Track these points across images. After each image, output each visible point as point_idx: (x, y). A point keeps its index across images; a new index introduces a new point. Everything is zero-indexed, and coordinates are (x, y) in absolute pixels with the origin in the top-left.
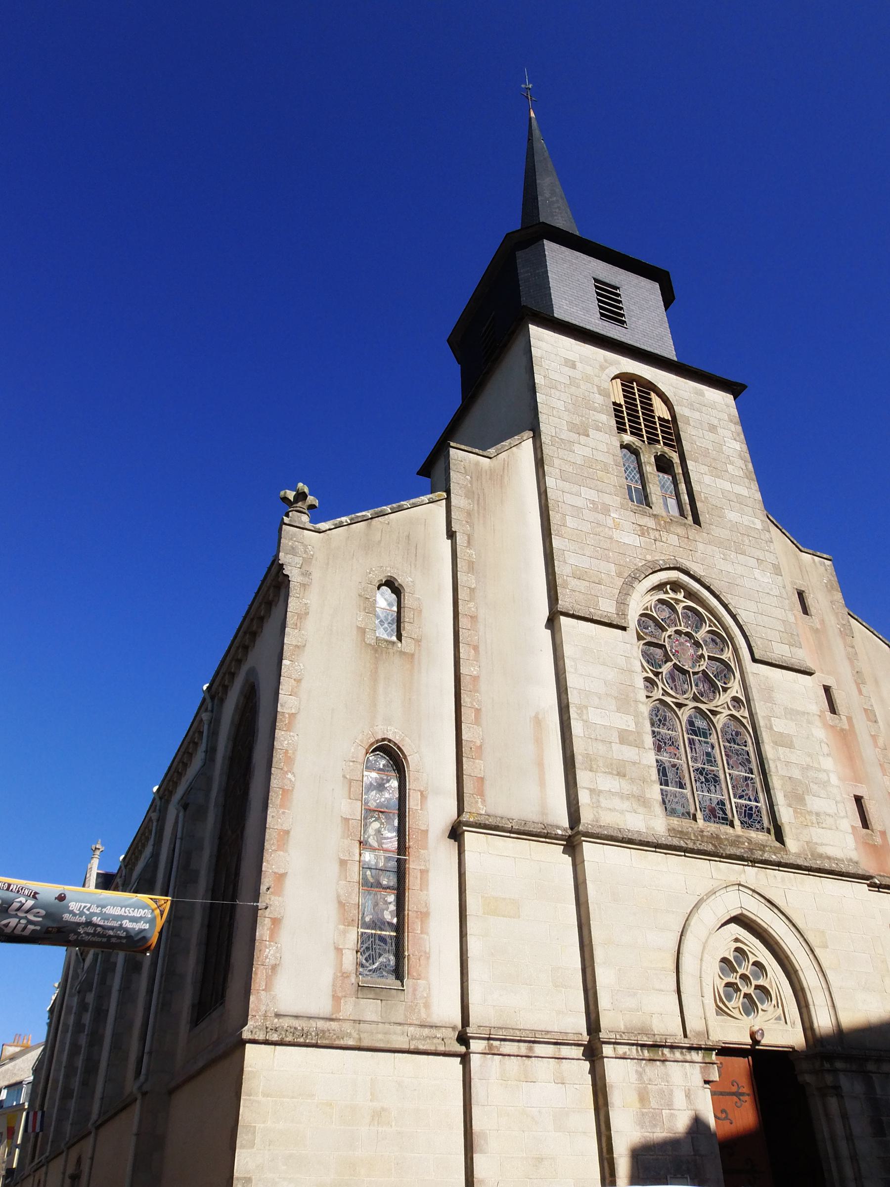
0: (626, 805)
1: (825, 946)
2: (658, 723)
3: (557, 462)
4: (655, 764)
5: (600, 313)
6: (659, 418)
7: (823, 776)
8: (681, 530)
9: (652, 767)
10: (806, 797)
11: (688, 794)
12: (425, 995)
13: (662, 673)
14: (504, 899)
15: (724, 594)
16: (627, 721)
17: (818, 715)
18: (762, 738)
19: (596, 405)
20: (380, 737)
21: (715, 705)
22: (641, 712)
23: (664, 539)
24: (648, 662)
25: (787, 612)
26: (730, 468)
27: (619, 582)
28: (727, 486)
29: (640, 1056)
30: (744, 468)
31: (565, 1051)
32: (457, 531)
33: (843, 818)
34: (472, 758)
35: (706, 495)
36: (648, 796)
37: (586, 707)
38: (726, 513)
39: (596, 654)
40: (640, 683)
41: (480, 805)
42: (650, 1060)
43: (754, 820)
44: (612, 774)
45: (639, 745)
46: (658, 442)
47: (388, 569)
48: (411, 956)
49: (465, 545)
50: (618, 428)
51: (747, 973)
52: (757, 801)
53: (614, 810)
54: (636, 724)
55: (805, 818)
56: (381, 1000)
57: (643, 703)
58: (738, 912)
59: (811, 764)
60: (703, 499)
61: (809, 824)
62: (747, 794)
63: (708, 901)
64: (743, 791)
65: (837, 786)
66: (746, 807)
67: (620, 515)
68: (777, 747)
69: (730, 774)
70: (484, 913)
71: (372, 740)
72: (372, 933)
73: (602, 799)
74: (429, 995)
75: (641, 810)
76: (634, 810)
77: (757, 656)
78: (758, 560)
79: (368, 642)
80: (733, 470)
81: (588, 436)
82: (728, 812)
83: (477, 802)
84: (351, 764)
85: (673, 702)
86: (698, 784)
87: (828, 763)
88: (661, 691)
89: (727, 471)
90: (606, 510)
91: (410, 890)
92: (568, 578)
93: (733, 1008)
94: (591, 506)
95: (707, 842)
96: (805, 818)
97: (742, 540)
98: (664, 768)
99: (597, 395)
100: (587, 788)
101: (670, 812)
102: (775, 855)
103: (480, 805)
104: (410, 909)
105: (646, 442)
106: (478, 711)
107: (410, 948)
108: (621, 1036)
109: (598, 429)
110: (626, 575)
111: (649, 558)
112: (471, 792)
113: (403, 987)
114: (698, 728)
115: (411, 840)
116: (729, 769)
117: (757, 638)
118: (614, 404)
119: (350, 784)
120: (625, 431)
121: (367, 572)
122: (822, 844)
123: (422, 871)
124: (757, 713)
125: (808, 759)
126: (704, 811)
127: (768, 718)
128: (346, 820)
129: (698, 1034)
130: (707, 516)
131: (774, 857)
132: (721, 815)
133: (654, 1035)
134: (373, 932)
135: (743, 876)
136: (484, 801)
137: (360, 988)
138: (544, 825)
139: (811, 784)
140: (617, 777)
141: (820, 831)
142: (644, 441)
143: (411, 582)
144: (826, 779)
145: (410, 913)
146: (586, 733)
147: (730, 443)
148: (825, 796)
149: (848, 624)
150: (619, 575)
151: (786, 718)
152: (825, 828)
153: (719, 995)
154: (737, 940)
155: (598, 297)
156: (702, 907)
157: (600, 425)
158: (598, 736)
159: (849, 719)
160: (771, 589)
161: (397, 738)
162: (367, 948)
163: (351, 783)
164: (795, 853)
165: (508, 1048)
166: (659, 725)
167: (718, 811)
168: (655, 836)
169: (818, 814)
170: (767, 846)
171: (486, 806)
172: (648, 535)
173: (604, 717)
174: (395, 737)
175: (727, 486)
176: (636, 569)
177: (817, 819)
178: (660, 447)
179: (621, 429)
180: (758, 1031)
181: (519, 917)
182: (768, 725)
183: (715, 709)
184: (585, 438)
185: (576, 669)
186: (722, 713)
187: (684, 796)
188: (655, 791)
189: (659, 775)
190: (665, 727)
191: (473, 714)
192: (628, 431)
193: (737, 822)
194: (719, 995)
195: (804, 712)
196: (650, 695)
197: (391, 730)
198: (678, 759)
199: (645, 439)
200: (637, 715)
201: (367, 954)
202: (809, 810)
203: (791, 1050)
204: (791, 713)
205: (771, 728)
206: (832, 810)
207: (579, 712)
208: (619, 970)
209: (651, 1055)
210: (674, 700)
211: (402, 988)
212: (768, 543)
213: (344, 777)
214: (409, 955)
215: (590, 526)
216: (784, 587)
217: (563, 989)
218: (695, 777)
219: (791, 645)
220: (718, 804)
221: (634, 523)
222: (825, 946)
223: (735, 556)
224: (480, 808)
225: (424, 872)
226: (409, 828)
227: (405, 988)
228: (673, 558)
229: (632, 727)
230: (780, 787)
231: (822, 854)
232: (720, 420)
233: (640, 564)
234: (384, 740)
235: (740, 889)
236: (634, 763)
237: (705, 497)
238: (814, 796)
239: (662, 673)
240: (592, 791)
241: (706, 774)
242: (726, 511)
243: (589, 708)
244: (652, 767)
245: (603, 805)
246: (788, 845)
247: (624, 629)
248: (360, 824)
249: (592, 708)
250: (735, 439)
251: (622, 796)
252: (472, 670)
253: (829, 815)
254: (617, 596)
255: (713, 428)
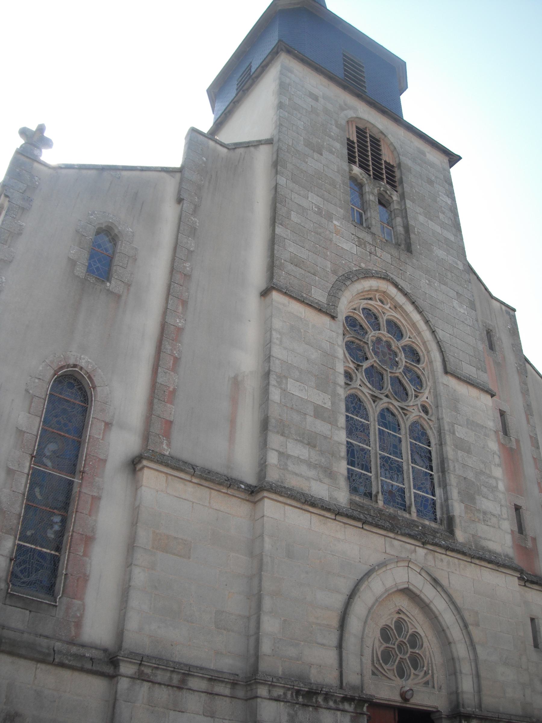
0: (312, 473)
1: (477, 625)
2: (353, 410)
3: (289, 166)
4: (345, 443)
5: (345, 74)
6: (385, 162)
7: (493, 482)
8: (395, 253)
9: (342, 444)
10: (477, 497)
11: (372, 477)
12: (79, 615)
13: (362, 366)
14: (175, 538)
15: (426, 313)
16: (324, 399)
17: (494, 431)
18: (445, 440)
19: (332, 134)
20: (72, 362)
21: (407, 405)
22: (338, 393)
23: (378, 254)
24: (350, 355)
25: (478, 341)
26: (441, 216)
27: (333, 279)
28: (438, 229)
29: (294, 700)
30: (453, 219)
31: (220, 688)
32: (185, 199)
33: (504, 519)
34: (164, 401)
35: (419, 230)
36: (335, 469)
37: (286, 378)
38: (435, 249)
39: (303, 334)
40: (341, 380)
41: (165, 446)
42: (303, 705)
43: (428, 510)
44: (302, 442)
45: (333, 423)
46: (382, 179)
47: (111, 216)
48: (69, 575)
49: (191, 212)
50: (349, 159)
51: (405, 641)
52: (433, 495)
53: (300, 475)
54: (333, 403)
55: (474, 514)
56: (30, 611)
57: (341, 386)
58: (406, 586)
59: (484, 470)
60: (416, 233)
61: (477, 520)
62: (425, 487)
63: (380, 572)
64: (422, 484)
65: (503, 493)
66: (423, 498)
67: (341, 224)
68: (456, 450)
69: (413, 467)
70: (153, 548)
71: (62, 363)
72: (31, 548)
73: (289, 463)
74: (82, 616)
75: (326, 480)
76: (320, 479)
77: (449, 370)
78: (457, 293)
79: (77, 274)
80: (444, 218)
81: (321, 154)
82: (407, 500)
83: (162, 443)
84: (37, 381)
85: (369, 393)
86: (383, 470)
87: (498, 472)
88: (359, 382)
89: (438, 217)
90: (330, 217)
91: (78, 514)
92: (285, 262)
93: (388, 669)
94: (316, 209)
95: (384, 520)
96: (474, 514)
97: (445, 274)
98: (353, 450)
99: (334, 127)
100: (277, 451)
101: (354, 490)
102: (444, 541)
103: (165, 446)
104: (75, 530)
105: (372, 177)
106: (176, 360)
107: (69, 567)
108: (278, 680)
109: (331, 152)
110: (340, 274)
111: (363, 265)
112: (158, 433)
113: (56, 602)
114: (389, 422)
115: (87, 466)
116: (412, 463)
117: (450, 356)
118: (348, 139)
119: (32, 399)
120: (355, 163)
121: (89, 213)
122: (485, 539)
123: (93, 497)
124: (443, 418)
125: (482, 466)
126: (385, 495)
127: (452, 425)
128: (20, 432)
129: (353, 688)
130: (418, 247)
131: (443, 543)
132: (399, 500)
133: (311, 683)
134: (33, 546)
135: (413, 555)
136: (169, 445)
137: (8, 595)
138: (228, 478)
139: (482, 487)
140: (307, 446)
141: (485, 527)
142: (370, 175)
143: (131, 232)
144: (495, 484)
145: (74, 534)
146: (283, 400)
147: (443, 197)
148: (492, 499)
149: (523, 365)
150: (334, 272)
151: (467, 427)
152: (489, 526)
153: (377, 654)
154: (399, 612)
155: (345, 72)
156: (372, 576)
157: (334, 150)
158: (294, 406)
159: (518, 441)
160: (466, 319)
161: (90, 367)
162: (24, 562)
163: (33, 398)
164: (461, 543)
165: (160, 676)
166: (353, 412)
167: (398, 497)
168: (337, 506)
169: (485, 513)
170: (438, 533)
171: (170, 448)
172: (365, 247)
173: (302, 390)
174: (88, 366)
175: (438, 229)
176: (351, 272)
177: (484, 517)
178: (384, 184)
179: (351, 160)
180: (408, 691)
181: (189, 558)
182: (452, 430)
183: (406, 408)
184: (319, 155)
185: (281, 342)
186: (398, 406)
187: (368, 479)
188: (342, 467)
189: (347, 456)
190: (359, 415)
191: (172, 362)
192: (357, 163)
193: (413, 509)
194: (377, 654)
195: (483, 426)
196: (349, 383)
197: (84, 359)
198: (367, 445)
199: (371, 174)
200: (334, 395)
201: (23, 567)
202: (478, 508)
203: (434, 710)
204: (471, 424)
205: (454, 433)
206: (497, 511)
207: (278, 380)
208: (285, 621)
209: (306, 701)
210: (371, 392)
211: (54, 604)
212: (467, 282)
213: (27, 391)
214: (66, 574)
215: (312, 225)
216: (477, 321)
217: (225, 632)
218: (380, 464)
219: (478, 369)
220: (398, 491)
221: (353, 234)
222: (477, 625)
223: (438, 285)
224: (164, 449)
225: (96, 499)
226: (86, 454)
227: (57, 604)
228: (384, 271)
229: (328, 405)
230: (455, 484)
231: (484, 547)
232: (436, 177)
233: (355, 269)
234: (75, 366)
235: (410, 566)
236: (326, 437)
237: (418, 232)
238: (483, 497)
239: (362, 366)
240: (281, 454)
241: (391, 462)
242: (435, 248)
243: (289, 379)
244: (342, 444)
245: (290, 468)
246: (456, 535)
247: (333, 317)
248: (35, 439)
249: (291, 380)
250: (448, 196)
251: (310, 465)
252: (178, 321)
253: (494, 515)
254: (329, 289)
255: (431, 182)
